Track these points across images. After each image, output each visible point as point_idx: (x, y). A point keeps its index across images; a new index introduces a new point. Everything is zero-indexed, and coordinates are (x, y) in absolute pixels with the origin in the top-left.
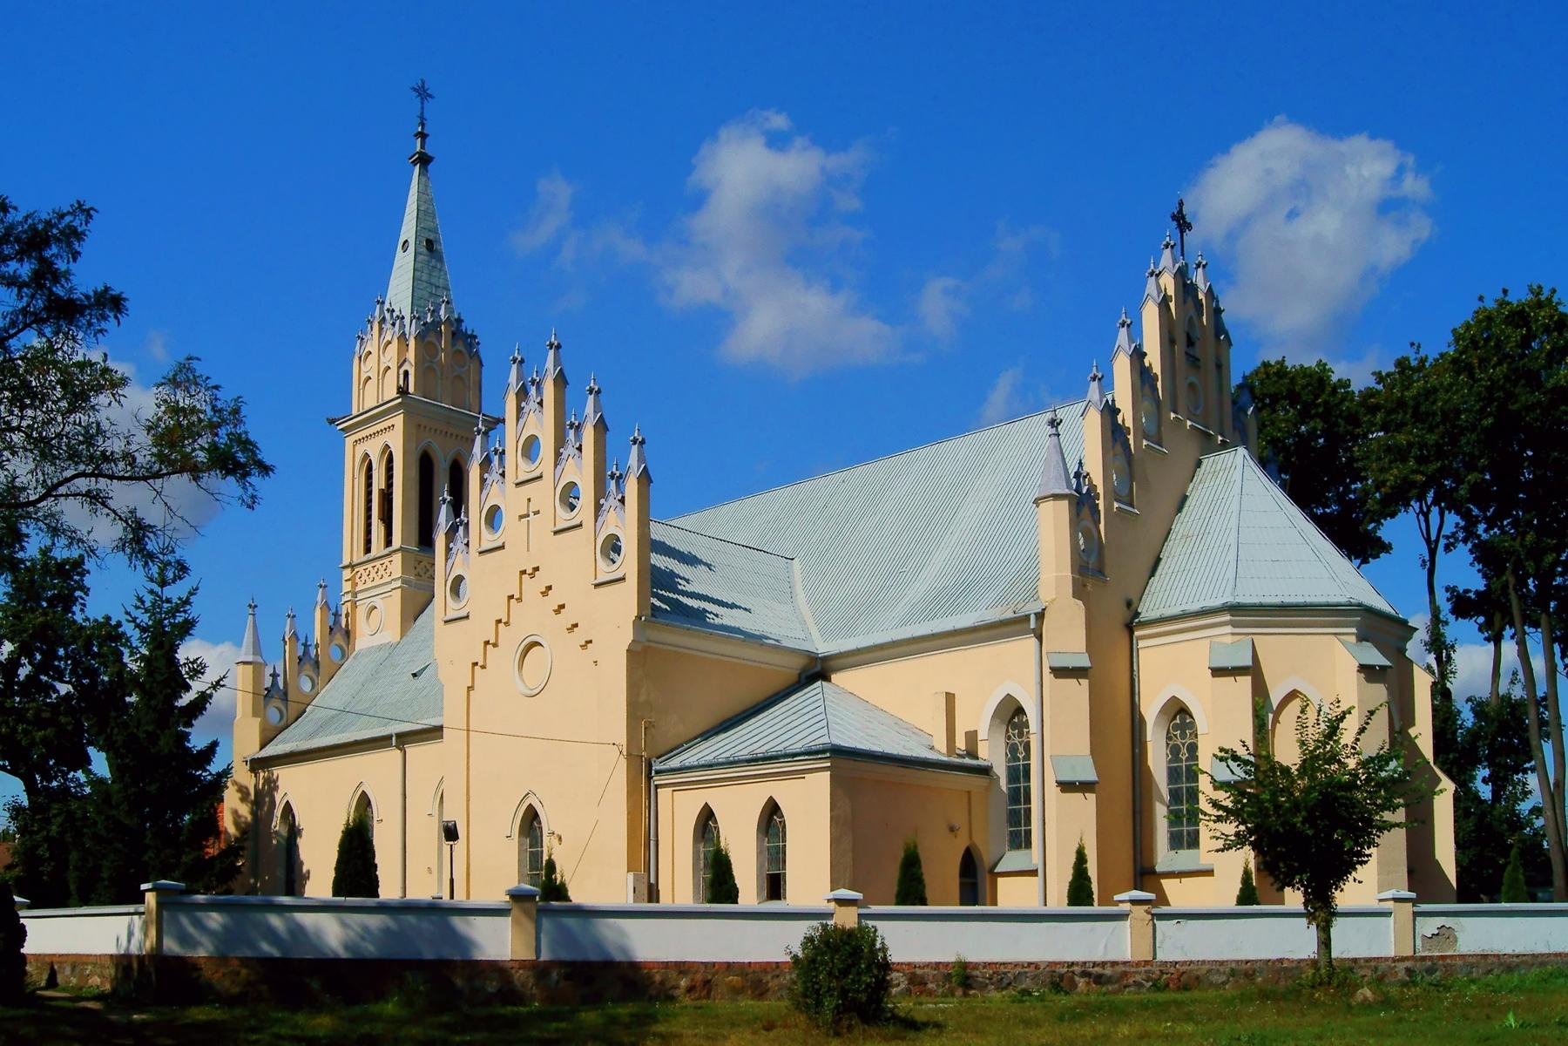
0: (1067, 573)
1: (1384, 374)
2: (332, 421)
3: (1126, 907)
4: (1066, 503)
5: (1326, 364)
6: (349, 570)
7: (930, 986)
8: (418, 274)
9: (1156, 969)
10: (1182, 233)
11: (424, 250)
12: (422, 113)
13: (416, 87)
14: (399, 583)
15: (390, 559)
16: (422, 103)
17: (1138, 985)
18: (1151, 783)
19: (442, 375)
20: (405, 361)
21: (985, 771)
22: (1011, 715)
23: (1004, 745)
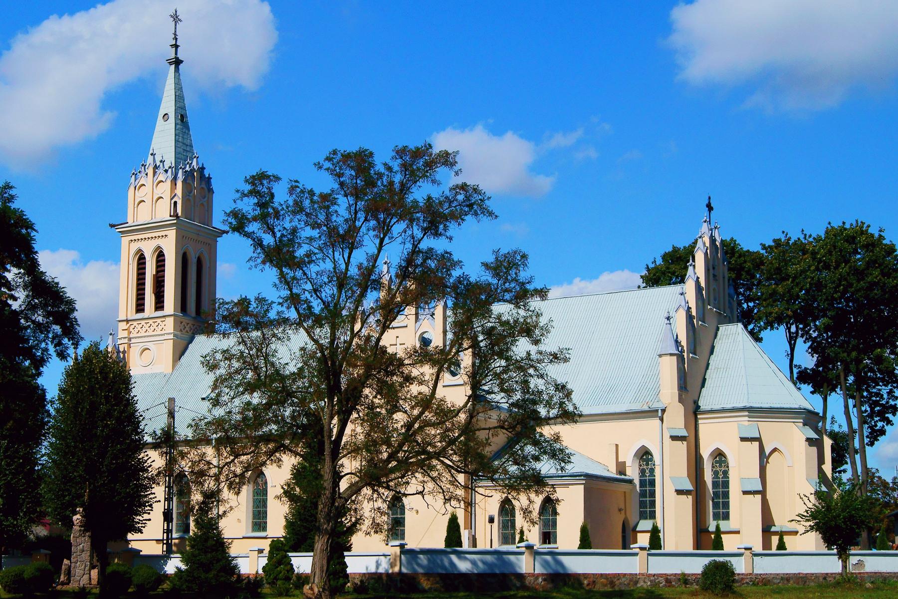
0: (676, 391)
1: (767, 246)
2: (112, 226)
3: (637, 550)
4: (675, 357)
5: (735, 240)
6: (125, 323)
7: (673, 583)
8: (177, 137)
9: (754, 577)
10: (710, 212)
11: (179, 122)
12: (175, 31)
13: (172, 15)
14: (172, 336)
15: (164, 319)
16: (176, 25)
17: (747, 583)
18: (705, 489)
19: (194, 204)
20: (175, 195)
21: (630, 482)
22: (644, 455)
23: (638, 469)
